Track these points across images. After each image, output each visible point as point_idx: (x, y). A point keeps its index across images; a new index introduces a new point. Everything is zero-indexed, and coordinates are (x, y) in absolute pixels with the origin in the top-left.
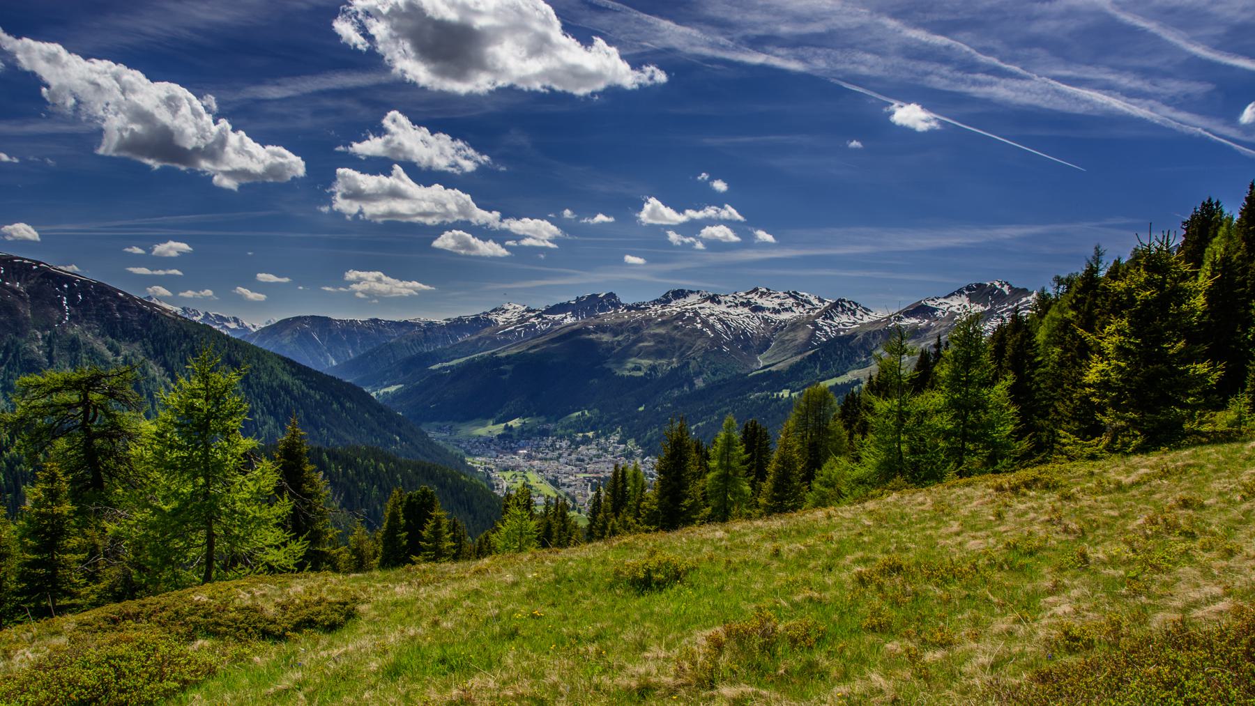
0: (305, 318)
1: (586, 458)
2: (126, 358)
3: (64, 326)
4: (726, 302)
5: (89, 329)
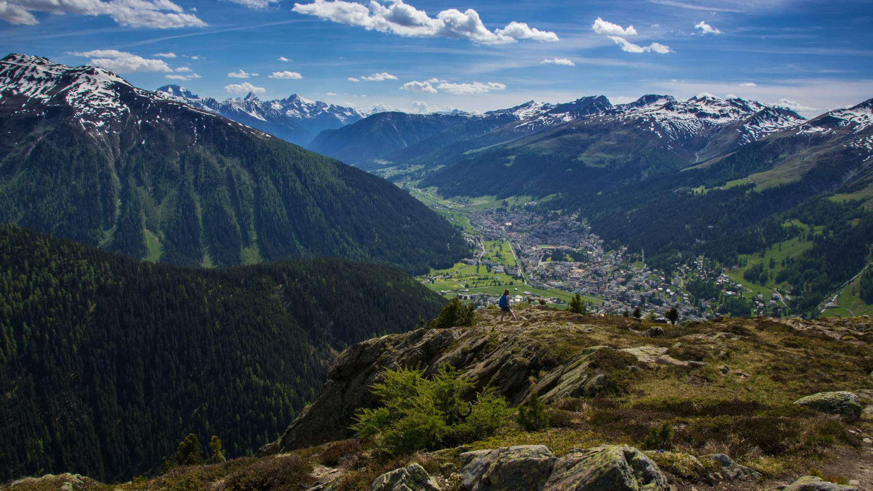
1: (550, 232)
2: (228, 169)
3: (193, 147)
4: (678, 109)
5: (208, 148)
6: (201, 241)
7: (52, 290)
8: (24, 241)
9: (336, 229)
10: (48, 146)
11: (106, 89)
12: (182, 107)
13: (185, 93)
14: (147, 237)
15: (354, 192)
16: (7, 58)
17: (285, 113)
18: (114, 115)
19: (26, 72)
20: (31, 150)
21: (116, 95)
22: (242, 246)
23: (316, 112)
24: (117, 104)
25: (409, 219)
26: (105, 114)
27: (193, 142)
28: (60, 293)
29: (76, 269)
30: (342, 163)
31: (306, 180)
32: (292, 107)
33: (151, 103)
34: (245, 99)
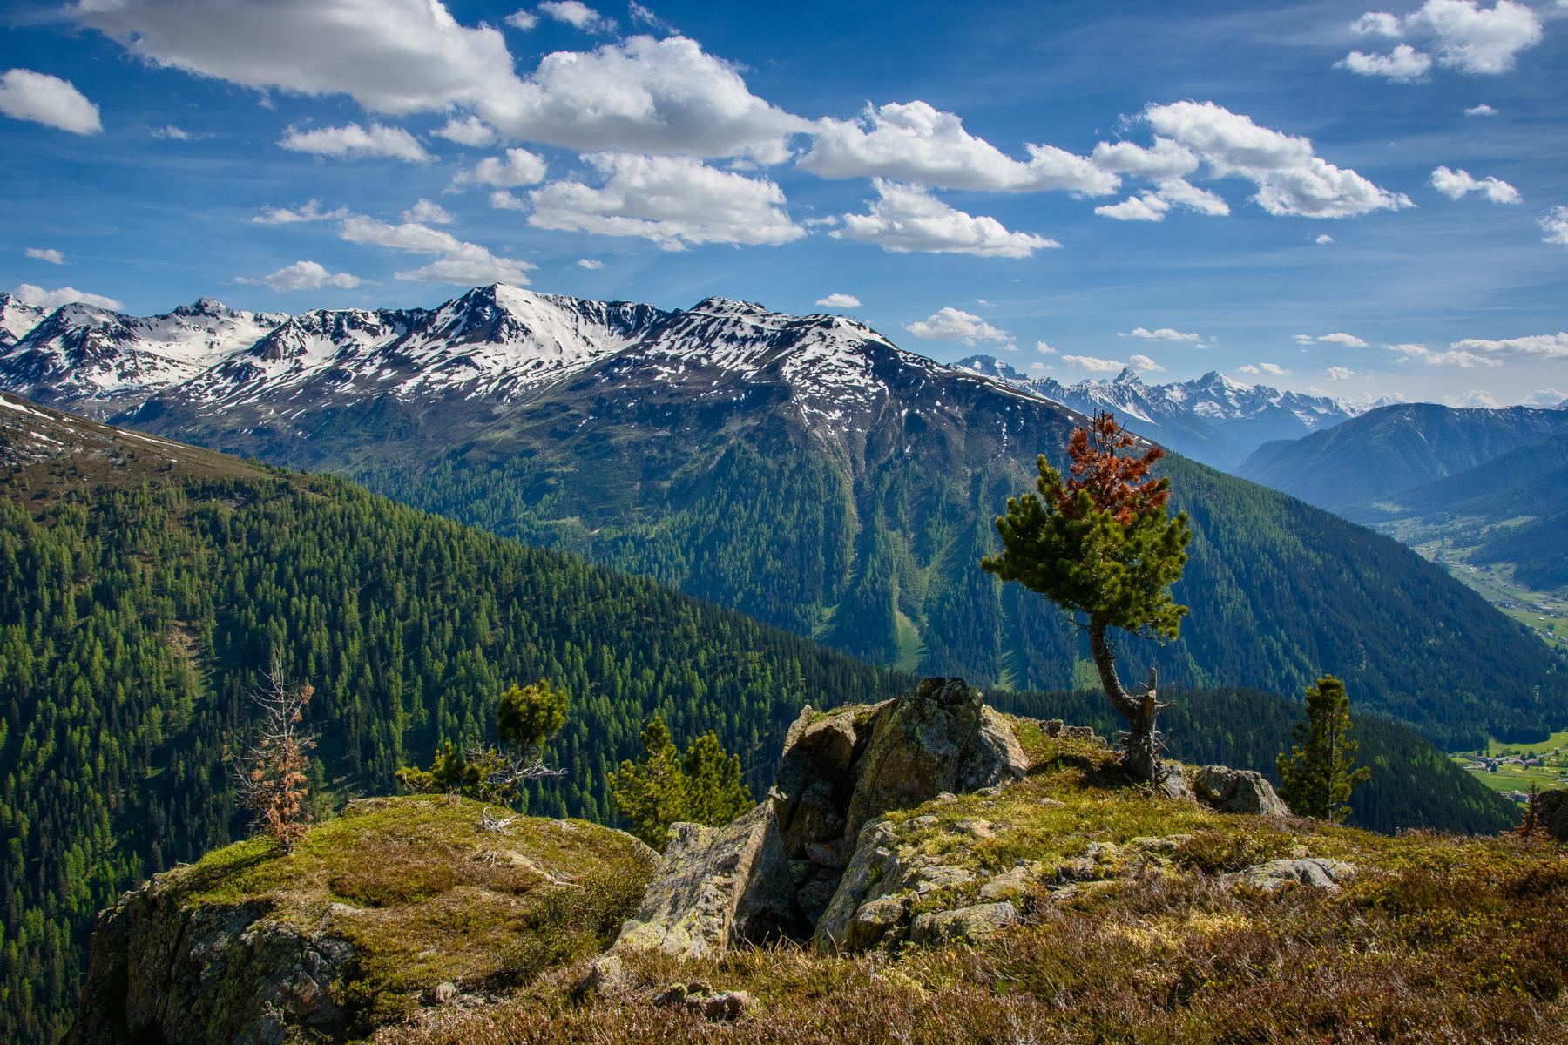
0: (1407, 407)
6: (998, 640)
7: (693, 703)
8: (659, 610)
9: (1277, 638)
10: (744, 453)
11: (851, 353)
12: (982, 386)
13: (1003, 370)
14: (898, 625)
15: (1319, 562)
16: (698, 307)
17: (1191, 408)
18: (861, 399)
19: (725, 327)
20: (717, 458)
21: (867, 364)
22: (1077, 657)
23: (1254, 406)
24: (868, 380)
25: (1442, 625)
26: (846, 397)
27: (1000, 452)
28: (706, 708)
29: (740, 668)
30: (1297, 502)
31: (1217, 533)
32: (1206, 397)
33: (927, 379)
34: (1115, 381)
